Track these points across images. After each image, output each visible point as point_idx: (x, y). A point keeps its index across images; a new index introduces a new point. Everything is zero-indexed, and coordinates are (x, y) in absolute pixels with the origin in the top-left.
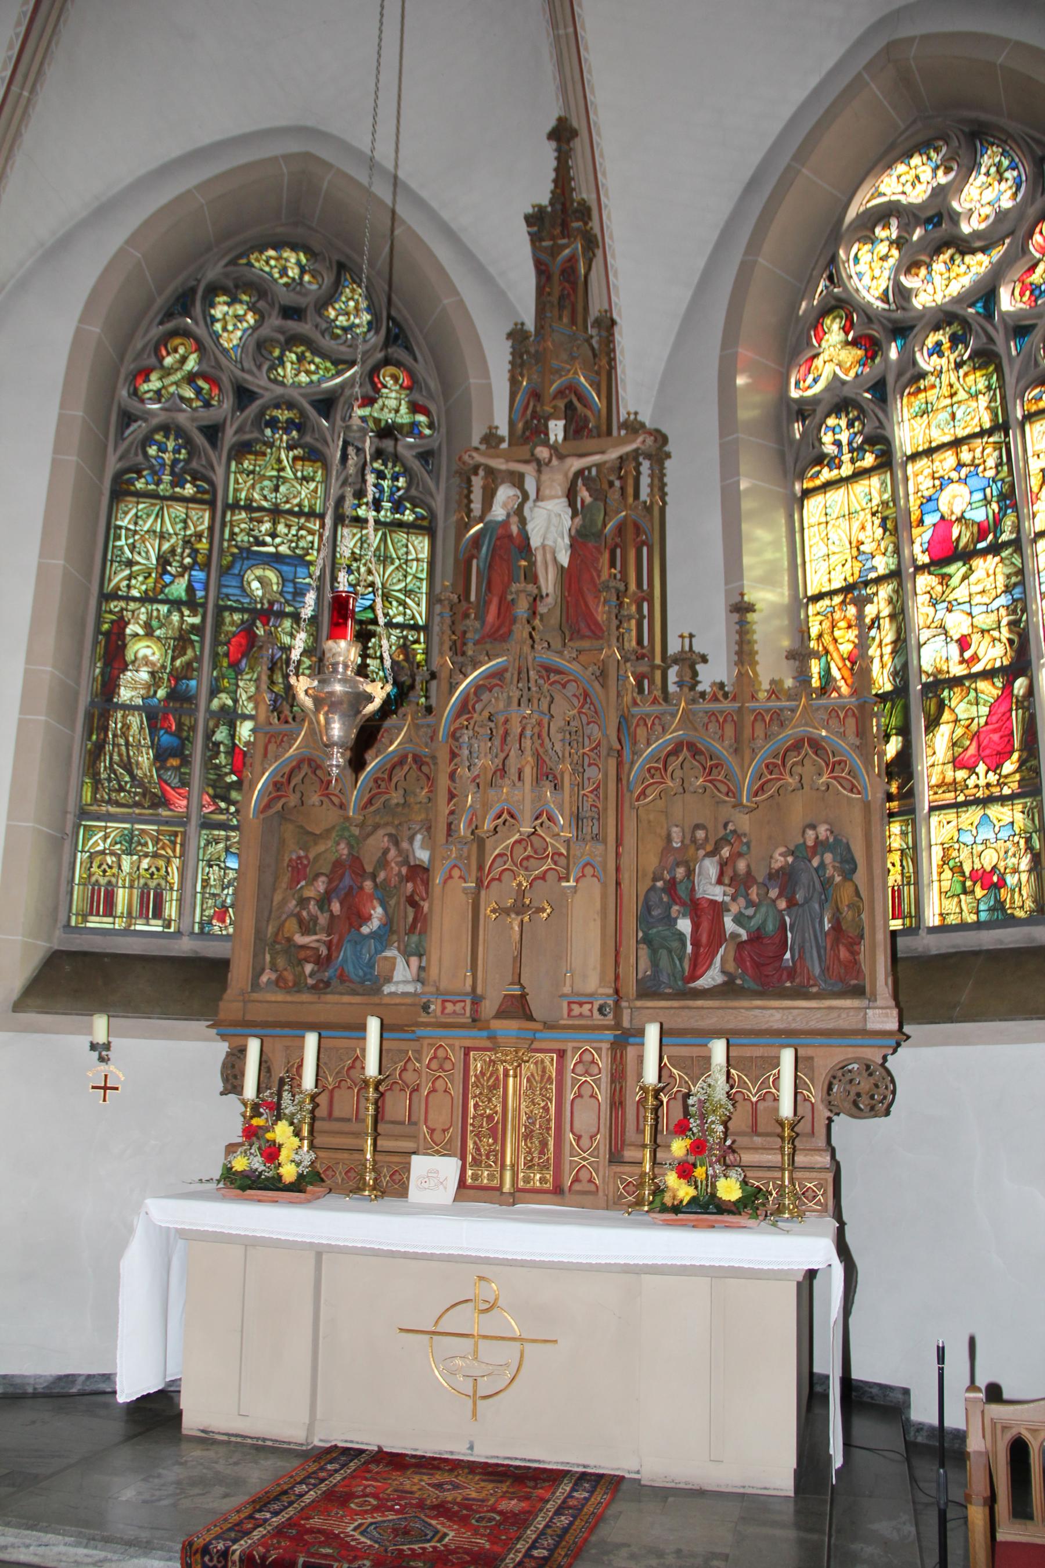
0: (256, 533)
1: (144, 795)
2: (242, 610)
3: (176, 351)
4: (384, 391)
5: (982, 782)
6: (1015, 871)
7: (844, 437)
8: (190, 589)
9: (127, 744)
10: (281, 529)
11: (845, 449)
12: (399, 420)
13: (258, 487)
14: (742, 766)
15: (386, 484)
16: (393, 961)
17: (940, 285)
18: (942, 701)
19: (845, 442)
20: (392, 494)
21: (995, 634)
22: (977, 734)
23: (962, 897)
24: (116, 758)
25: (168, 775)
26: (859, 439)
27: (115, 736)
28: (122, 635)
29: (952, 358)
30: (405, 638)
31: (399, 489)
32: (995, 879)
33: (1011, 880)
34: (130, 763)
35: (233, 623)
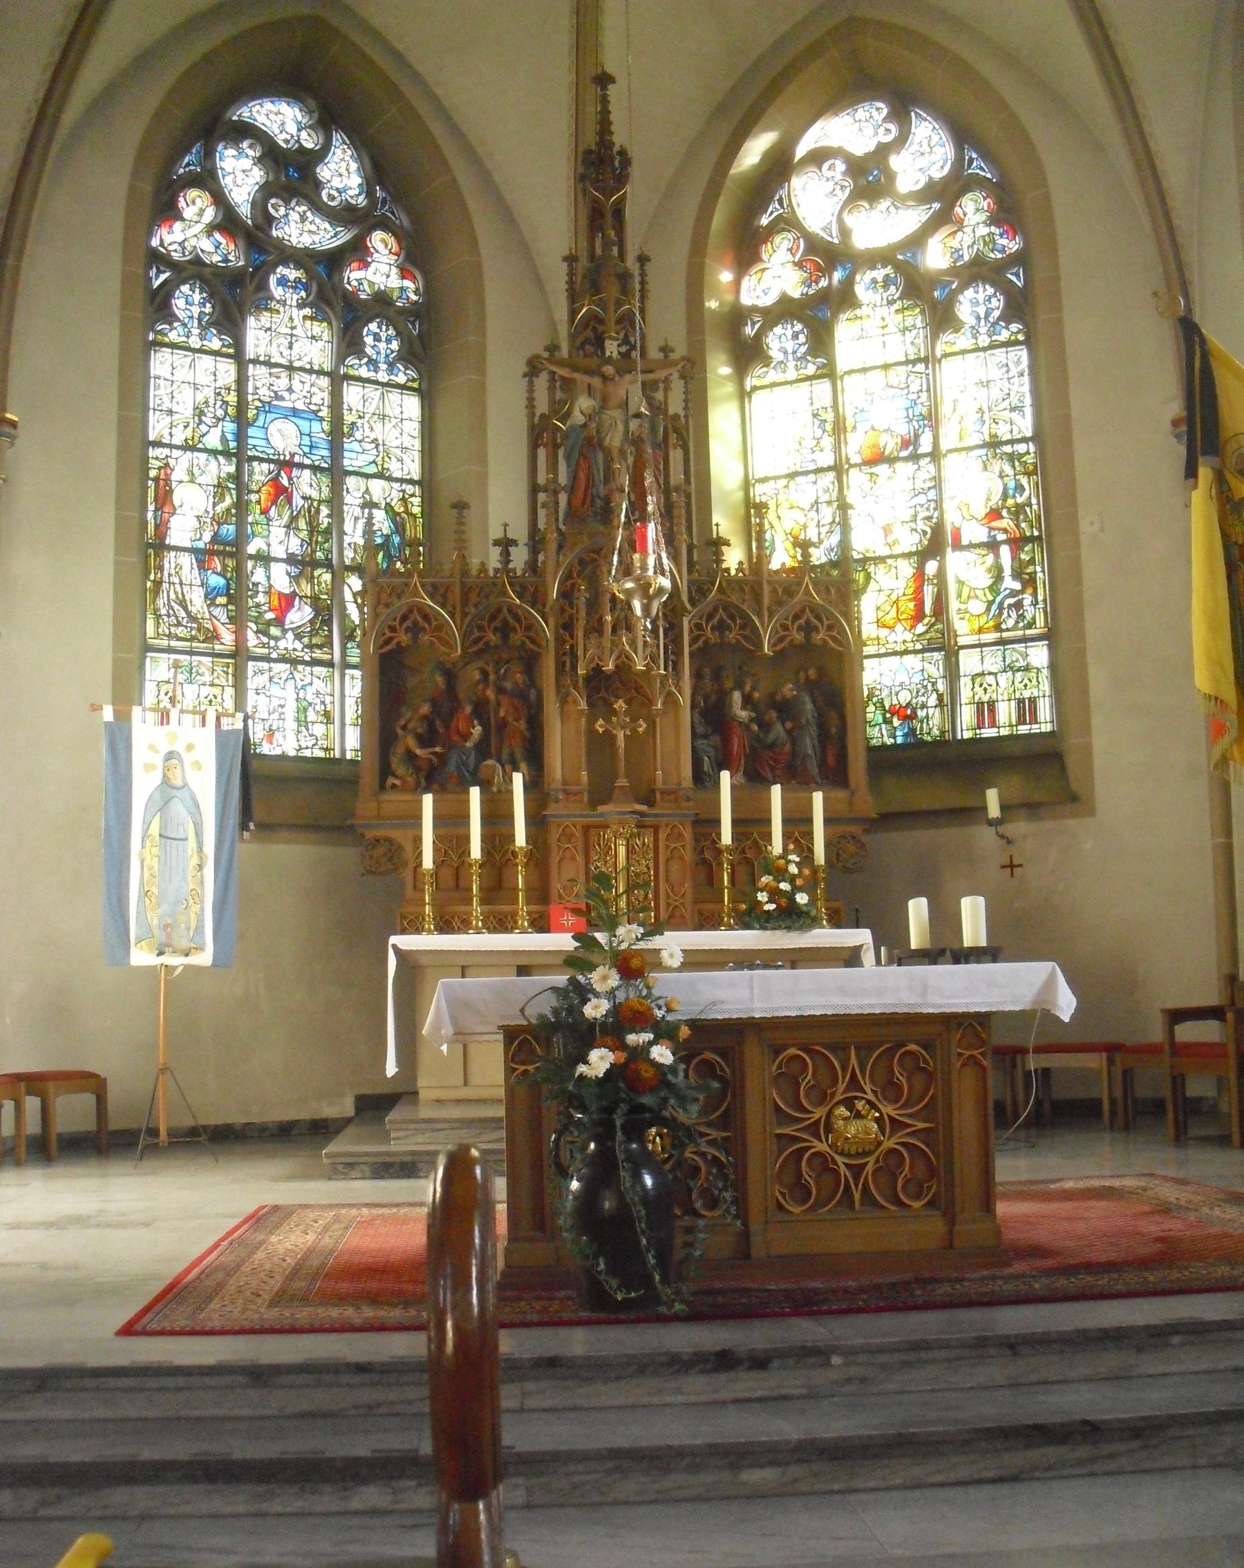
0: (275, 388)
1: (199, 630)
2: (269, 461)
3: (194, 203)
4: (376, 255)
5: (900, 640)
6: (924, 706)
7: (790, 346)
8: (224, 439)
9: (181, 584)
10: (296, 385)
11: (790, 357)
12: (389, 285)
13: (274, 344)
14: (763, 625)
15: (382, 346)
16: (494, 768)
17: (877, 228)
18: (869, 574)
19: (790, 351)
20: (387, 356)
21: (913, 525)
22: (896, 602)
23: (883, 726)
24: (173, 596)
25: (217, 611)
26: (803, 349)
27: (170, 575)
28: (168, 480)
29: (885, 295)
30: (404, 491)
31: (393, 352)
32: (909, 712)
33: (921, 714)
34: (185, 600)
35: (262, 473)
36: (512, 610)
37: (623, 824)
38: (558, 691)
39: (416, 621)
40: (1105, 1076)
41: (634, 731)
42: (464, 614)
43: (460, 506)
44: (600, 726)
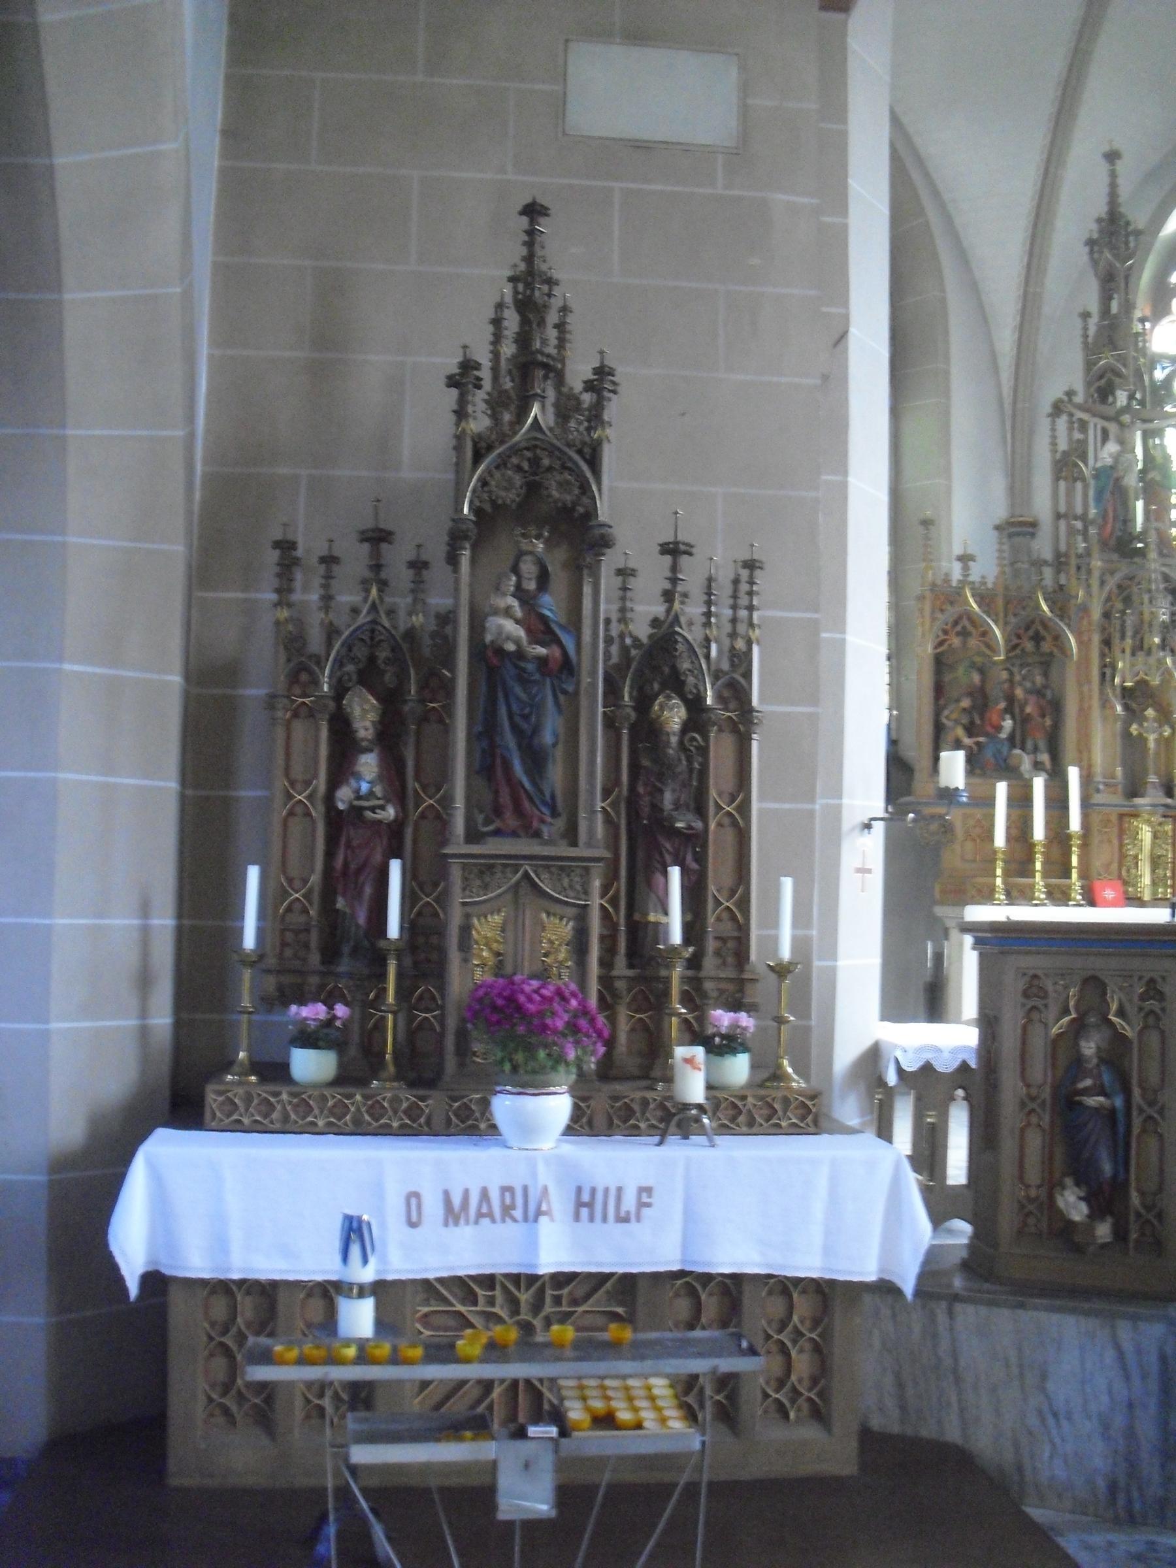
36: (1044, 623)
37: (1152, 814)
38: (1101, 699)
39: (964, 626)
40: (980, 934)
41: (1161, 734)
42: (1006, 623)
43: (926, 523)
44: (1134, 729)
